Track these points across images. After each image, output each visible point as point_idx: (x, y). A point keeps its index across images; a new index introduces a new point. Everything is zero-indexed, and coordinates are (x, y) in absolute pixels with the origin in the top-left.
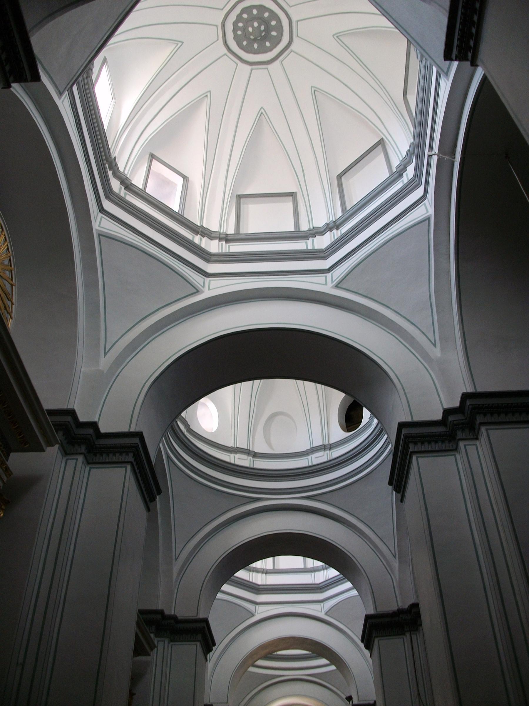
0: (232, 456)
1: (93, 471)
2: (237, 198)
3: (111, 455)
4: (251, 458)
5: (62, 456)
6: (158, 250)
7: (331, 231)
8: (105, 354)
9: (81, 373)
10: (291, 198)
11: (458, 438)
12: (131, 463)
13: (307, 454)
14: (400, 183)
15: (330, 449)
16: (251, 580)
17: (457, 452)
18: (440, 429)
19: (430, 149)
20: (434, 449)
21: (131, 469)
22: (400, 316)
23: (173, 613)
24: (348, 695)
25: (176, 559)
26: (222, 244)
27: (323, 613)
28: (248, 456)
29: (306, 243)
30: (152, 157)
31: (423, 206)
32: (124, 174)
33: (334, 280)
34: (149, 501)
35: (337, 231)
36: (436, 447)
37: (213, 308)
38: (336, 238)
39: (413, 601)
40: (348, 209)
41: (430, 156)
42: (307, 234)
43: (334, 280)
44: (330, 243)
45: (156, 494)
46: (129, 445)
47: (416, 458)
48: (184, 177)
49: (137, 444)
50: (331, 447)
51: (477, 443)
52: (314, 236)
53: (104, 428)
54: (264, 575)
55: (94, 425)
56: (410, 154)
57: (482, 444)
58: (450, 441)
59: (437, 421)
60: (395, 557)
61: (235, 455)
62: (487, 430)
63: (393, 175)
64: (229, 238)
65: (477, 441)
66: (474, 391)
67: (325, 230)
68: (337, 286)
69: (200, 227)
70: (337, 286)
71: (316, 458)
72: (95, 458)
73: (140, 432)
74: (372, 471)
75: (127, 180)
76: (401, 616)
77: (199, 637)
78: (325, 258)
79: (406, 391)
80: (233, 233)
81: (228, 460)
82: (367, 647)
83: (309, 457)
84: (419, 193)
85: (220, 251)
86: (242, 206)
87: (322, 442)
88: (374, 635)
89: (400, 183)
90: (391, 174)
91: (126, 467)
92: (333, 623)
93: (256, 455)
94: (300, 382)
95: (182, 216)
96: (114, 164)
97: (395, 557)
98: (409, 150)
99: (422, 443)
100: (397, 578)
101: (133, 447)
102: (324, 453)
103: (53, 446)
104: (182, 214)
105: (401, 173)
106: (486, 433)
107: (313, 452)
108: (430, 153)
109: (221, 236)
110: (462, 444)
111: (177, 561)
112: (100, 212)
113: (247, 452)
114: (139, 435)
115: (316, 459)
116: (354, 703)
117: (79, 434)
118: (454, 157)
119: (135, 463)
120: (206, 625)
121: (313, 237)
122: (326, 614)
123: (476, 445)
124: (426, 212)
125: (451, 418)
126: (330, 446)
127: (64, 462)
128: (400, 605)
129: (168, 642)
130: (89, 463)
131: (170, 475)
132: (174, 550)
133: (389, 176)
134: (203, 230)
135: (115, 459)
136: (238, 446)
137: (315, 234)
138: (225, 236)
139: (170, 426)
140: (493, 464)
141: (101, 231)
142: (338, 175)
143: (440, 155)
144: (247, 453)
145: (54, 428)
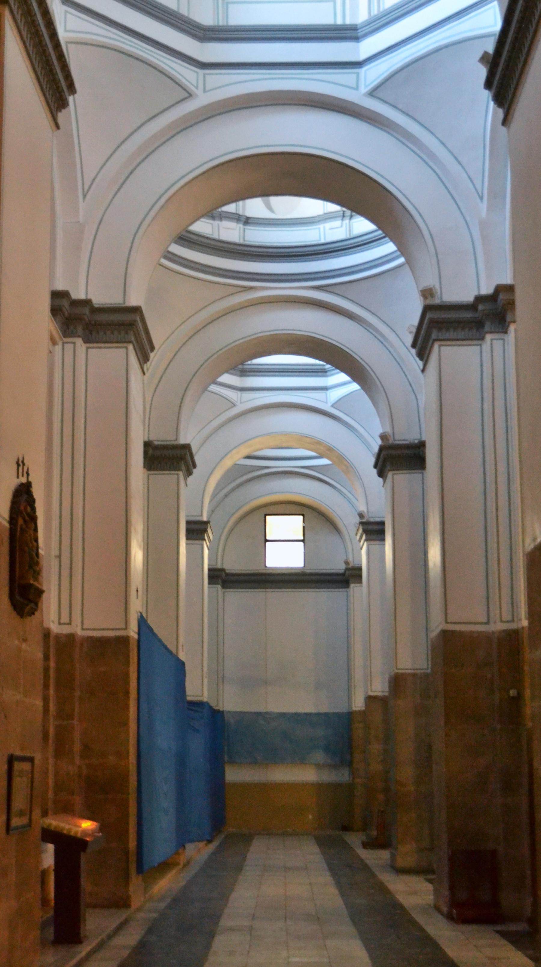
8: (84, 196)
28: (237, 223)
45: (149, 351)
61: (219, 222)
70: (372, 93)
71: (331, 229)
92: (342, 308)
110: (488, 337)
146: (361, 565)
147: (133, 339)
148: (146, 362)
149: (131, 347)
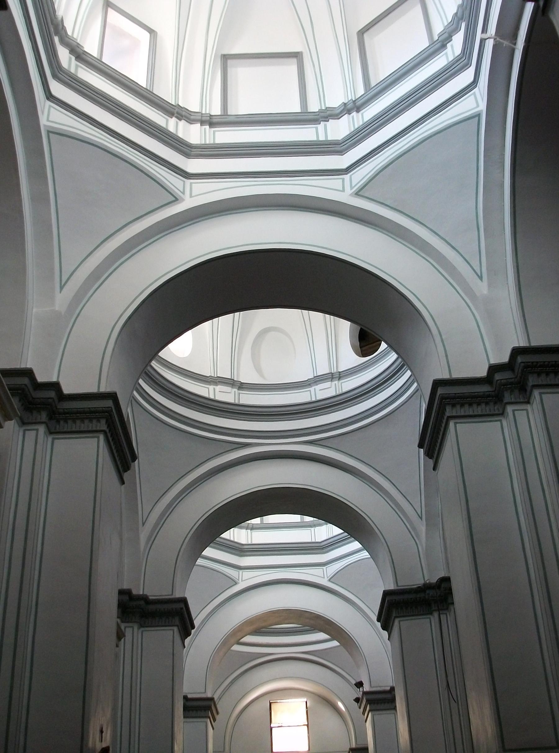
0: (211, 387)
1: (56, 441)
2: (223, 58)
3: (78, 422)
4: (236, 390)
5: (19, 426)
6: (121, 146)
7: (350, 114)
9: (33, 314)
10: (295, 60)
11: (505, 402)
12: (104, 432)
13: (309, 385)
14: (442, 56)
15: (340, 378)
16: (232, 539)
17: (504, 417)
18: (485, 389)
19: (484, 30)
20: (476, 413)
21: (104, 440)
22: (438, 237)
23: (141, 593)
24: (358, 681)
25: (143, 524)
26: (205, 129)
27: (326, 579)
29: (317, 129)
30: (108, 5)
31: (473, 96)
32: (72, 38)
33: (353, 186)
34: (123, 471)
35: (357, 114)
36: (478, 410)
37: (197, 220)
38: (356, 127)
39: (442, 574)
40: (372, 86)
41: (483, 41)
42: (318, 117)
43: (353, 186)
44: (348, 133)
46: (101, 409)
47: (453, 424)
48: (151, 31)
49: (110, 408)
50: (341, 376)
51: (529, 407)
52: (327, 119)
53: (66, 390)
54: (249, 531)
55: (55, 386)
56: (457, 19)
57: (534, 408)
58: (495, 403)
59: (481, 378)
60: (421, 518)
61: (215, 387)
62: (541, 394)
63: (433, 45)
64: (215, 120)
65: (529, 405)
66: (528, 345)
67: (341, 112)
68: (358, 194)
69: (175, 106)
70: (358, 194)
72: (58, 426)
73: (114, 393)
74: (394, 410)
75: (78, 47)
76: (427, 592)
77: (177, 620)
78: (341, 153)
79: (443, 337)
80: (219, 114)
81: (206, 395)
82: (384, 628)
83: (312, 389)
84: (467, 77)
85: (203, 142)
86: (229, 69)
87: (328, 370)
88: (394, 615)
89: (442, 56)
90: (431, 43)
91: (98, 438)
93: (242, 386)
94: (305, 312)
95: (150, 91)
96: (61, 27)
97: (421, 518)
98: (456, 14)
99: (462, 405)
100: (424, 545)
101: (107, 412)
102: (331, 385)
103: (11, 420)
104: (151, 90)
105: (445, 43)
106: (539, 397)
107: (317, 383)
108: (484, 36)
109: (204, 119)
110: (509, 409)
111: (144, 526)
112: (47, 99)
113: (231, 383)
114: (113, 396)
115: (321, 391)
116: (365, 690)
117: (38, 398)
118: (515, 42)
119: (108, 431)
120: (185, 607)
121: (325, 121)
122: (329, 580)
123: (527, 410)
124: (475, 105)
125: (498, 377)
126: (340, 375)
127: (21, 434)
128: (426, 579)
129: (138, 628)
130: (51, 433)
131: (134, 419)
132: (140, 513)
133: (428, 45)
134: (180, 112)
135: (83, 427)
136: (218, 376)
137: (329, 118)
138: (209, 118)
139: (144, 372)
140: (546, 435)
141: (50, 127)
142: (359, 31)
143: (498, 39)
144: (231, 384)
145: (10, 393)
146: (368, 744)
147: (104, 427)
148: (126, 471)
149: (176, 629)
